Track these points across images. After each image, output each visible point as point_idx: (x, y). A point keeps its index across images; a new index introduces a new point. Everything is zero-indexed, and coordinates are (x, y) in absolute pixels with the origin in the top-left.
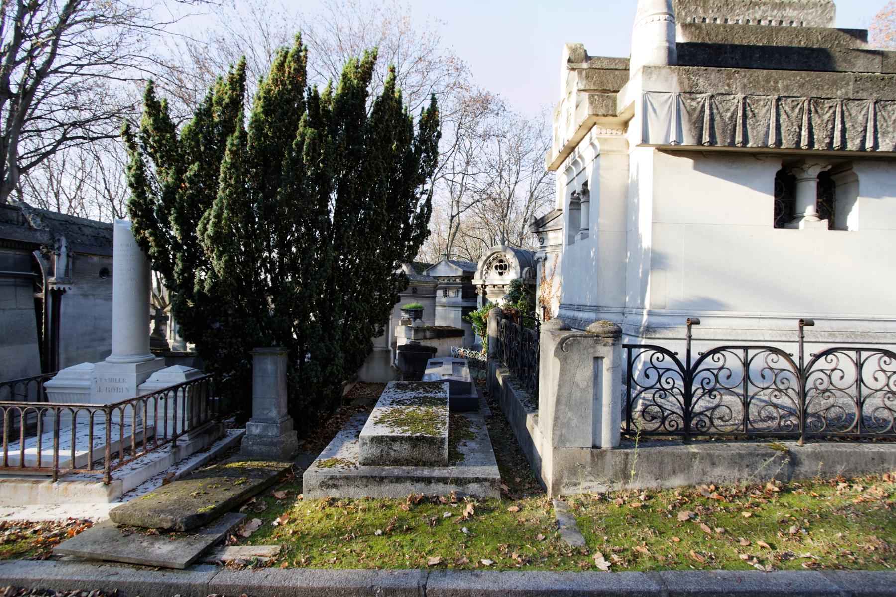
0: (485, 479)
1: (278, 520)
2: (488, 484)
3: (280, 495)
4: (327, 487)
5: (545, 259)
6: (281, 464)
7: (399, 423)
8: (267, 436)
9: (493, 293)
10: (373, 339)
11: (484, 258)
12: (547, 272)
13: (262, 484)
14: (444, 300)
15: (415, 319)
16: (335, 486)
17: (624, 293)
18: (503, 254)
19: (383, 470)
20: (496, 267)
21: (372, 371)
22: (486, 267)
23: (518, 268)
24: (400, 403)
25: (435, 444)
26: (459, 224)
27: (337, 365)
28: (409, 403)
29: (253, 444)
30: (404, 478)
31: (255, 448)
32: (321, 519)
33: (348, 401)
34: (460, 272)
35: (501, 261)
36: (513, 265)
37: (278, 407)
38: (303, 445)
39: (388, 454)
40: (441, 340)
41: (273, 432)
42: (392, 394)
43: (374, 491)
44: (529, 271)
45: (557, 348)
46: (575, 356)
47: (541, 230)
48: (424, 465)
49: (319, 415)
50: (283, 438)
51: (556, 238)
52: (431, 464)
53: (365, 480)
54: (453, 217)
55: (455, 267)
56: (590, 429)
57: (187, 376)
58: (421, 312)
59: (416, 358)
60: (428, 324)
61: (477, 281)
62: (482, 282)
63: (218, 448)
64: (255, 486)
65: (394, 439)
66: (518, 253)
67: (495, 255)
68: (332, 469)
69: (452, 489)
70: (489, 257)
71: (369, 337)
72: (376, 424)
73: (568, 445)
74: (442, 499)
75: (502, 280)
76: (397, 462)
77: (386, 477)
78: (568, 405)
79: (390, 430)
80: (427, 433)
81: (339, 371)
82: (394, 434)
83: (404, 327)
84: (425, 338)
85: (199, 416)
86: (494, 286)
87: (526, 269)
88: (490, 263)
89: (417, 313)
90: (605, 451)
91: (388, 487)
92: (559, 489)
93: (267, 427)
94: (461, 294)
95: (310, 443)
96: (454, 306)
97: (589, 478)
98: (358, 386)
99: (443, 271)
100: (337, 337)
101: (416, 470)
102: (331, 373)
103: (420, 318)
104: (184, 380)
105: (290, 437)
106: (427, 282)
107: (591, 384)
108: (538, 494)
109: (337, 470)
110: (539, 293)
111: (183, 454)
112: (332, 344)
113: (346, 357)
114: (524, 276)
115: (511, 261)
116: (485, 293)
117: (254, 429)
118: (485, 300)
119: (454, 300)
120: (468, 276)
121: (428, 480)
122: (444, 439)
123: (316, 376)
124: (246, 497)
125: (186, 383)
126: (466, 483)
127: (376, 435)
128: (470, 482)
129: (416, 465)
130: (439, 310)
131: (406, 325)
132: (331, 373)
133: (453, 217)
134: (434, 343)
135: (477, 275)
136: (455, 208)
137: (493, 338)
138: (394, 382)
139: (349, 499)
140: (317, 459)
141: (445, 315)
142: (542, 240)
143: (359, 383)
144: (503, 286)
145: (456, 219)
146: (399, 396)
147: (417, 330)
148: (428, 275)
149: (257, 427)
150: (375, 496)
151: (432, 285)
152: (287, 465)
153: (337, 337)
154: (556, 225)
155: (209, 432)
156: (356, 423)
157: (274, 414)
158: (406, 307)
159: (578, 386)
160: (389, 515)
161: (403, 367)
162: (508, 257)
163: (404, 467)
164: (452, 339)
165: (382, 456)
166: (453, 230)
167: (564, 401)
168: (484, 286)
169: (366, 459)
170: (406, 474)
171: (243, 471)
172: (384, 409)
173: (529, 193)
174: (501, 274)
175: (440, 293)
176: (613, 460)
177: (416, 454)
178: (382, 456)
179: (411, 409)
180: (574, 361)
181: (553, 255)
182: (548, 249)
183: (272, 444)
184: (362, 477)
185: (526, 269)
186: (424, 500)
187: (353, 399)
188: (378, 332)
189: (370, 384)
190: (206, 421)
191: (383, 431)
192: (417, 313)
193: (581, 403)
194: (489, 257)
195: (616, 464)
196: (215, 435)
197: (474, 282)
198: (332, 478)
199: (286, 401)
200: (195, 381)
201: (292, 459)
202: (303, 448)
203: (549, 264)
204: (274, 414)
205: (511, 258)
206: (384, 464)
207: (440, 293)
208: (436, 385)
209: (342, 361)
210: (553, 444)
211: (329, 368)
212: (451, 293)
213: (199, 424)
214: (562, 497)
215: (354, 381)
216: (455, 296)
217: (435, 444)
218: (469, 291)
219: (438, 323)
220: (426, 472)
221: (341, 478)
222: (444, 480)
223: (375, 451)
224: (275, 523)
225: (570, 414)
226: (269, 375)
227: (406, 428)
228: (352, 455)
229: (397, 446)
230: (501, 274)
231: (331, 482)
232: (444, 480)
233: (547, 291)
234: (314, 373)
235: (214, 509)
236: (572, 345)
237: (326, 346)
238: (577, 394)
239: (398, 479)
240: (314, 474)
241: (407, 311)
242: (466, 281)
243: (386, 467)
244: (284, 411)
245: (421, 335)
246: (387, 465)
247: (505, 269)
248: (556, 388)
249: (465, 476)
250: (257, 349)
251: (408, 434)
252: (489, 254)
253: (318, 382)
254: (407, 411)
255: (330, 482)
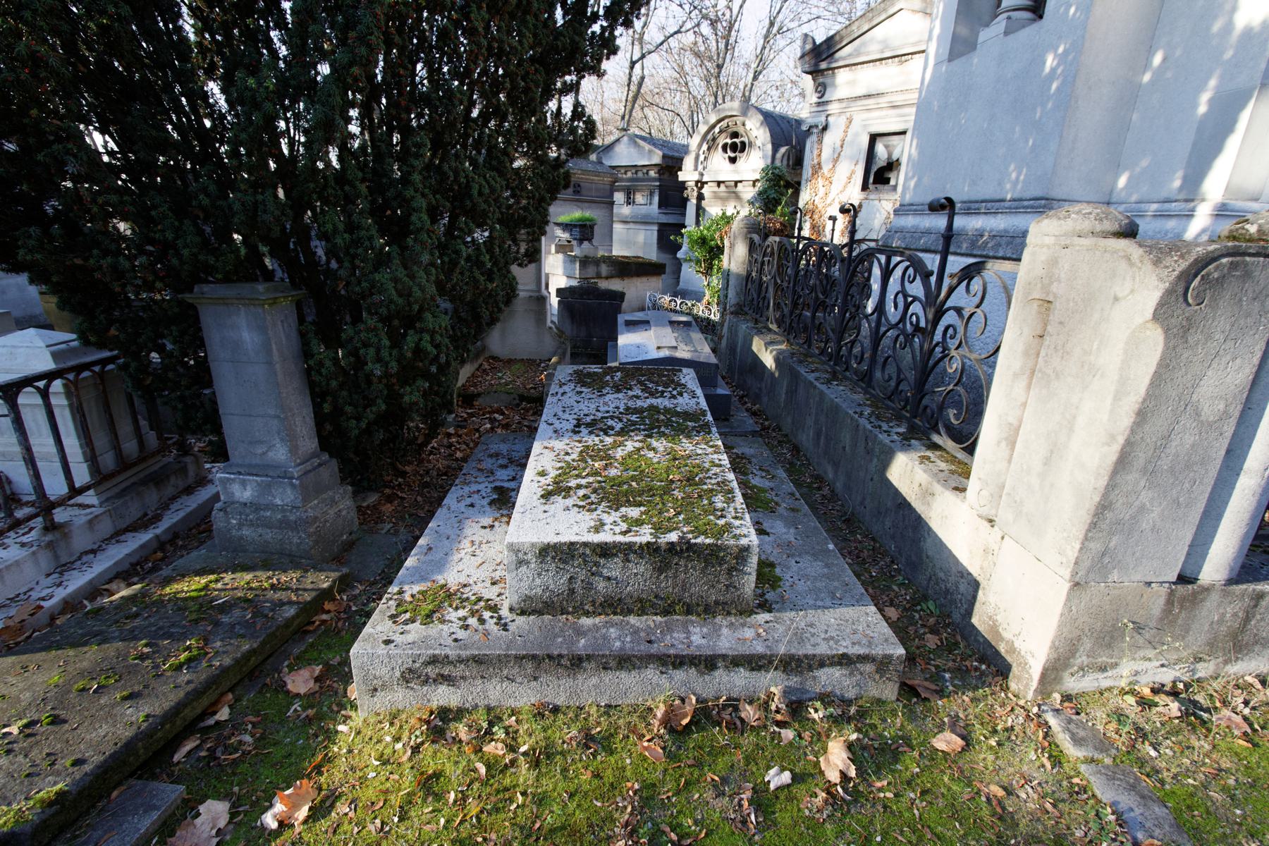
0: (864, 659)
1: (279, 807)
2: (869, 668)
3: (300, 682)
4: (426, 682)
5: (825, 128)
6: (311, 577)
7: (614, 494)
8: (271, 507)
9: (716, 196)
10: (515, 269)
11: (703, 129)
12: (827, 153)
13: (252, 652)
14: (626, 211)
15: (581, 241)
16: (448, 680)
17: (1117, 169)
18: (739, 120)
19: (580, 632)
20: (725, 148)
21: (513, 337)
22: (705, 147)
23: (769, 147)
24: (596, 426)
25: (721, 561)
26: (643, 78)
27: (433, 333)
28: (618, 426)
29: (240, 525)
30: (641, 658)
31: (246, 532)
32: (409, 800)
33: (468, 399)
34: (657, 158)
35: (735, 135)
36: (759, 143)
37: (291, 439)
38: (374, 508)
39: (589, 586)
40: (627, 281)
41: (284, 496)
42: (570, 399)
43: (558, 690)
44: (788, 153)
45: (1169, 293)
46: (1220, 320)
47: (823, 65)
48: (689, 612)
49: (405, 445)
50: (314, 509)
51: (852, 83)
52: (708, 610)
53: (529, 667)
54: (633, 64)
55: (647, 147)
56: (1188, 535)
57: (56, 356)
58: (592, 227)
59: (592, 317)
60: (601, 253)
61: (687, 174)
62: (696, 177)
63: (181, 514)
64: (224, 671)
65: (605, 551)
66: (771, 120)
67: (724, 124)
68: (435, 629)
69: (774, 685)
70: (713, 126)
71: (507, 264)
72: (547, 496)
73: (1115, 576)
74: (750, 713)
75: (736, 172)
76: (613, 605)
77: (589, 658)
78: (1150, 472)
79: (588, 519)
80: (698, 532)
81: (437, 346)
82: (605, 537)
83: (560, 256)
84: (599, 276)
85: (116, 447)
86: (719, 183)
87: (783, 150)
88: (714, 139)
89: (584, 231)
90: (1207, 590)
91: (594, 680)
92: (1058, 680)
93: (269, 486)
94: (656, 199)
95: (390, 499)
96: (644, 221)
97: (1141, 653)
98: (486, 366)
99: (624, 155)
100: (425, 258)
101: (669, 629)
102: (418, 351)
103: (590, 240)
104: (48, 364)
105: (333, 502)
106: (597, 174)
107: (1236, 411)
108: (982, 681)
109: (446, 633)
110: (804, 198)
111: (81, 541)
112: (412, 277)
113: (456, 311)
114: (778, 163)
115: (754, 133)
116: (700, 197)
117: (235, 488)
118: (700, 210)
119: (644, 210)
120: (672, 164)
121: (708, 663)
122: (747, 549)
123: (379, 359)
124: (189, 713)
125: (50, 376)
126: (810, 668)
127: (554, 539)
128: (822, 665)
129: (666, 612)
130: (618, 228)
131: (564, 253)
132: (418, 351)
133: (633, 64)
134: (615, 285)
135: (688, 163)
136: (637, 47)
137: (738, 275)
138: (570, 369)
139: (489, 709)
140: (394, 589)
141: (630, 238)
142: (821, 89)
143: (487, 360)
144: (736, 183)
145: (638, 66)
146: (590, 405)
147: (585, 262)
148: (600, 162)
149: (244, 484)
150: (560, 701)
151: (608, 179)
152: (324, 580)
153: (425, 258)
154: (857, 53)
155: (157, 479)
156: (488, 463)
157: (280, 453)
158: (564, 219)
159: (1198, 414)
160: (609, 776)
161: (568, 328)
162: (749, 125)
163: (633, 619)
164: (644, 279)
165: (572, 591)
166: (633, 88)
167: (1141, 457)
168: (700, 184)
169: (528, 598)
170: (644, 648)
171: (204, 611)
172: (559, 445)
173: (767, 23)
174: (733, 160)
175: (619, 197)
176: (1217, 612)
177: (666, 585)
178: (572, 591)
179: (630, 446)
180: (1209, 337)
181: (842, 120)
182: (833, 108)
183: (285, 524)
184: (519, 659)
185: (783, 150)
186: (705, 715)
187: (479, 395)
188: (526, 254)
189: (510, 362)
190: (145, 455)
191: (570, 524)
192: (584, 231)
193: (1188, 466)
194: (713, 126)
195: (1221, 621)
196: (176, 483)
197: (682, 176)
198: (434, 660)
199: (310, 421)
200: (79, 369)
201: (337, 560)
202: (369, 517)
203: (830, 139)
204: (280, 453)
205: (756, 131)
206: (580, 611)
207: (619, 197)
208: (660, 372)
209: (445, 321)
210: (1074, 573)
211: (411, 339)
212: (639, 198)
213: (124, 465)
214: (1067, 698)
215: (477, 356)
216: (648, 204)
217: (721, 561)
218: (672, 194)
219: (617, 251)
220: (697, 637)
221: (461, 661)
222: (755, 663)
223: (554, 581)
224: (270, 820)
225: (1145, 497)
226: (252, 351)
227: (634, 512)
228: (485, 573)
229: (613, 568)
230: (733, 160)
231: (430, 670)
232: (755, 663)
233: (822, 191)
234: (372, 351)
235: (60, 794)
236: (1221, 281)
237: (396, 280)
238: (1185, 439)
239: (625, 662)
240: (382, 650)
241: (566, 227)
242: (666, 176)
243: (586, 621)
244: (309, 443)
245: (591, 271)
246: (587, 614)
247: (743, 150)
248: (1126, 420)
249: (810, 650)
250: (206, 288)
251: (644, 535)
252: (713, 119)
253: (387, 375)
254: (619, 453)
255: (431, 671)
